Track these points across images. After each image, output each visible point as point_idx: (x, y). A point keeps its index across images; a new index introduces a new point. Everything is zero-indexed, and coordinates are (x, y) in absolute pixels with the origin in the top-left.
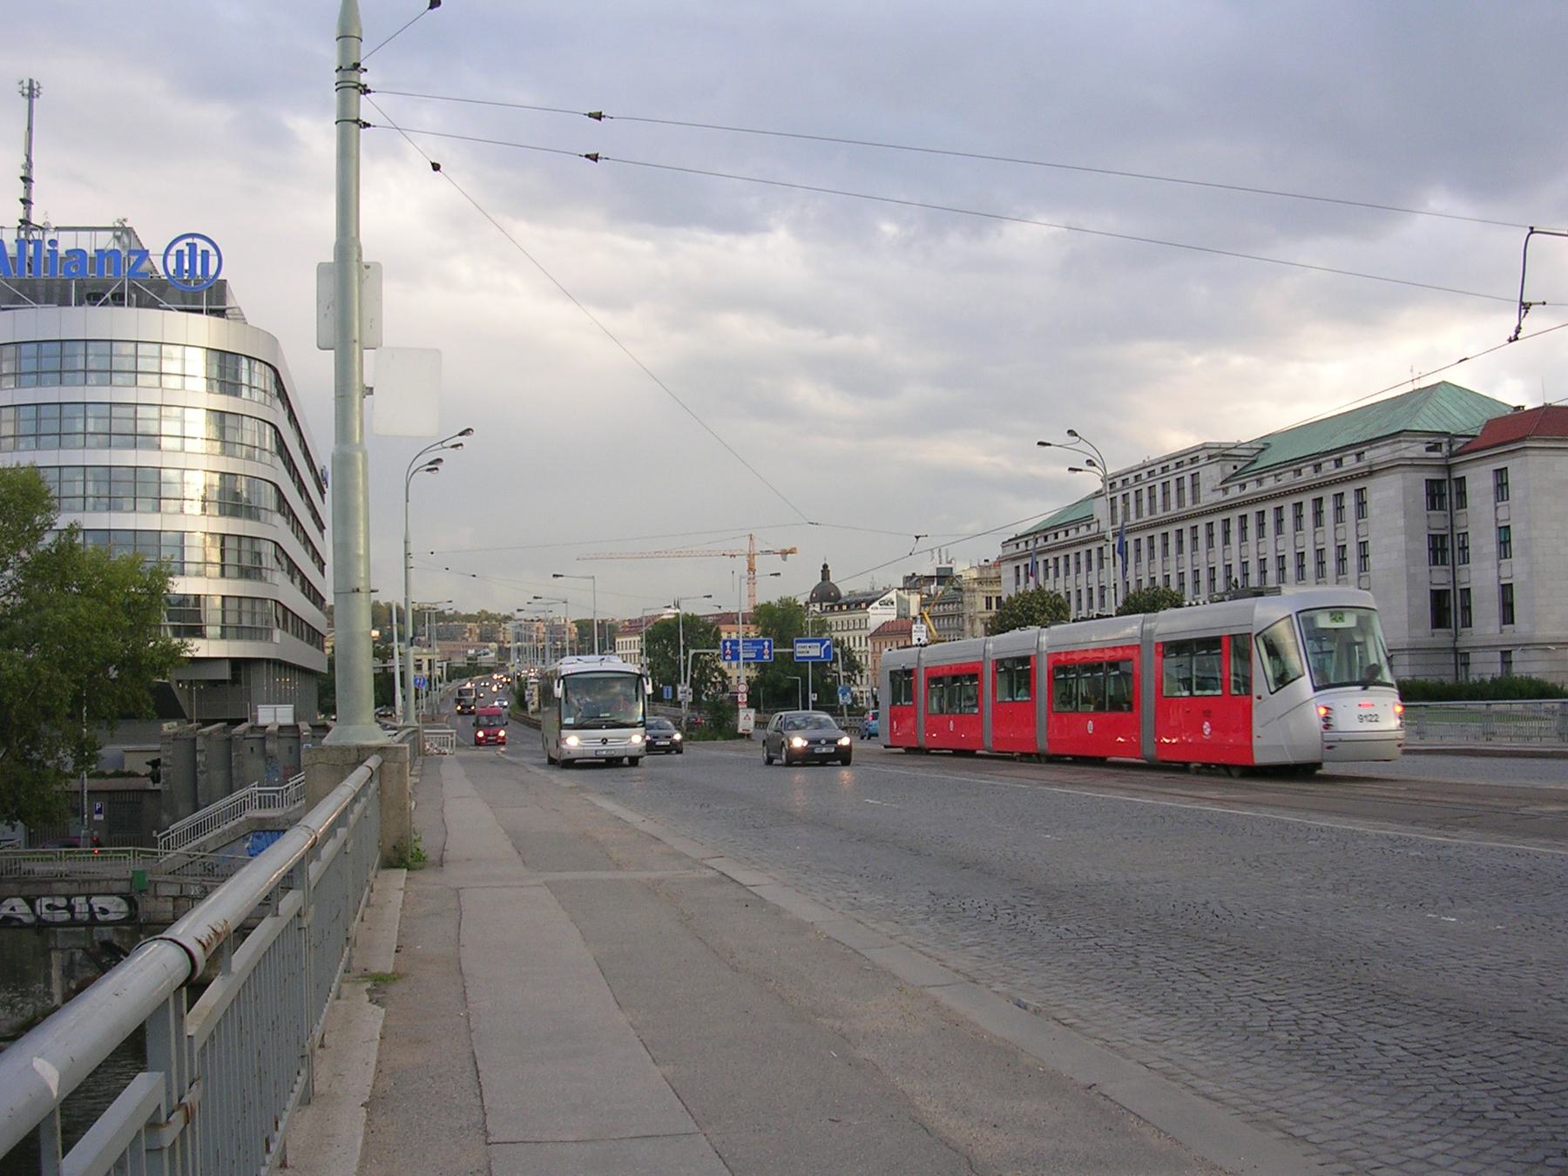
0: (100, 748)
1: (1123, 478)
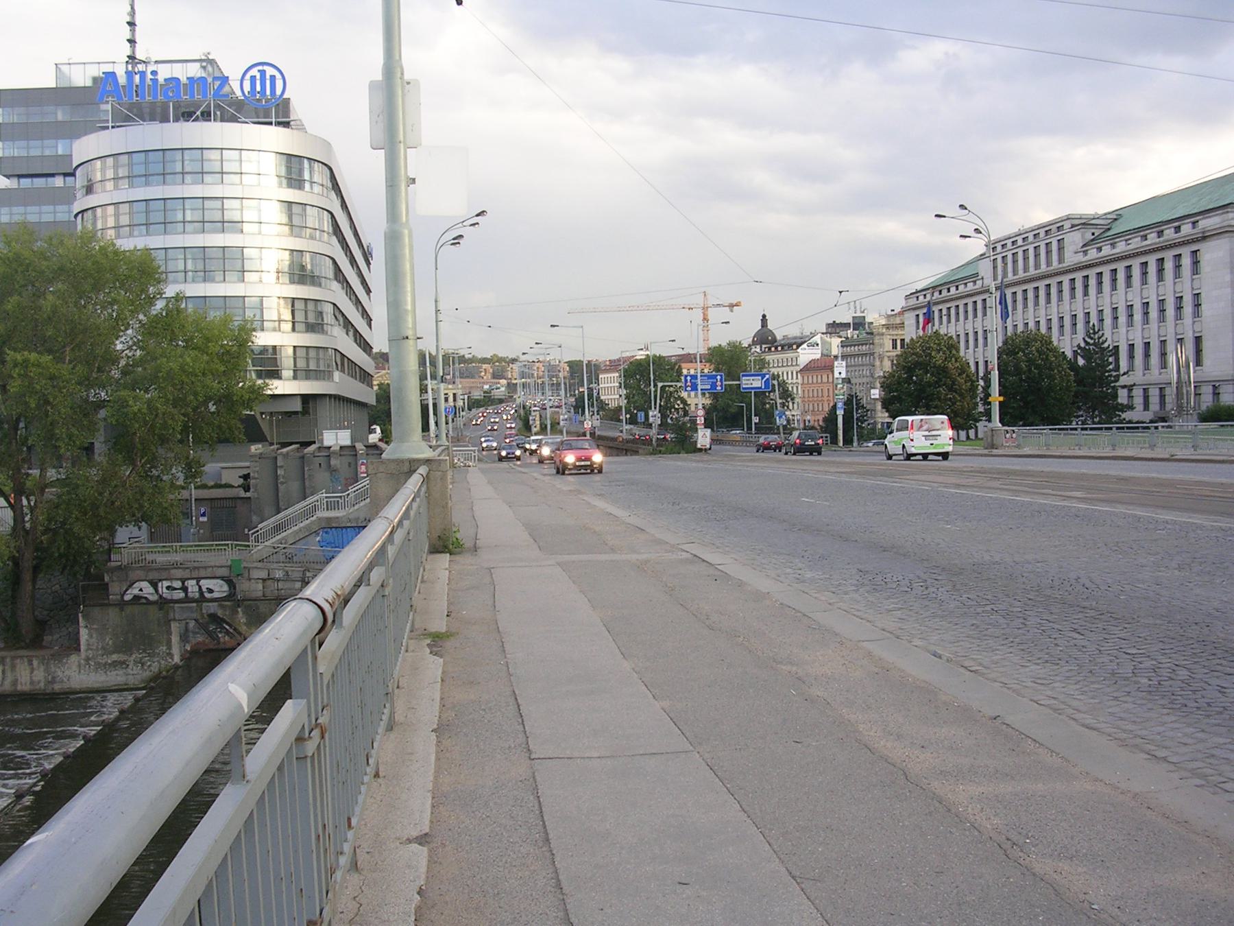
0: (204, 466)
1: (1003, 243)
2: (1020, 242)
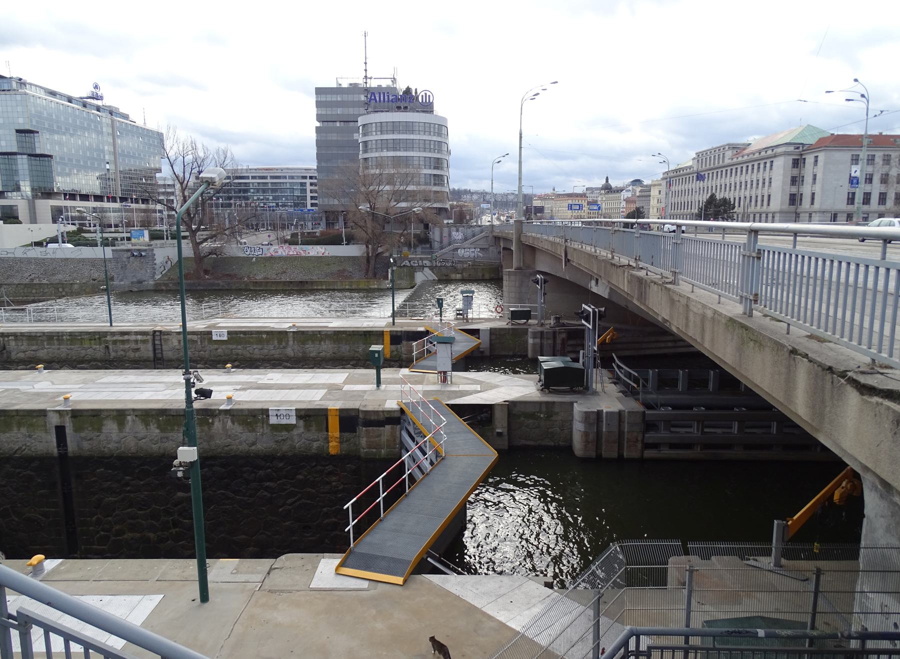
2: (709, 153)
